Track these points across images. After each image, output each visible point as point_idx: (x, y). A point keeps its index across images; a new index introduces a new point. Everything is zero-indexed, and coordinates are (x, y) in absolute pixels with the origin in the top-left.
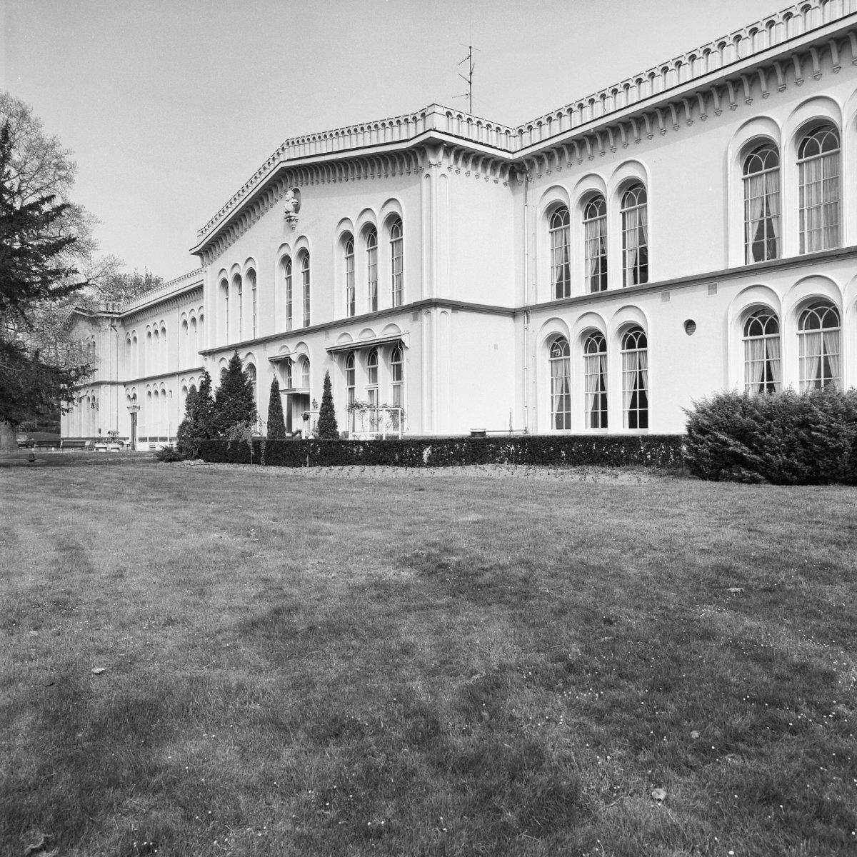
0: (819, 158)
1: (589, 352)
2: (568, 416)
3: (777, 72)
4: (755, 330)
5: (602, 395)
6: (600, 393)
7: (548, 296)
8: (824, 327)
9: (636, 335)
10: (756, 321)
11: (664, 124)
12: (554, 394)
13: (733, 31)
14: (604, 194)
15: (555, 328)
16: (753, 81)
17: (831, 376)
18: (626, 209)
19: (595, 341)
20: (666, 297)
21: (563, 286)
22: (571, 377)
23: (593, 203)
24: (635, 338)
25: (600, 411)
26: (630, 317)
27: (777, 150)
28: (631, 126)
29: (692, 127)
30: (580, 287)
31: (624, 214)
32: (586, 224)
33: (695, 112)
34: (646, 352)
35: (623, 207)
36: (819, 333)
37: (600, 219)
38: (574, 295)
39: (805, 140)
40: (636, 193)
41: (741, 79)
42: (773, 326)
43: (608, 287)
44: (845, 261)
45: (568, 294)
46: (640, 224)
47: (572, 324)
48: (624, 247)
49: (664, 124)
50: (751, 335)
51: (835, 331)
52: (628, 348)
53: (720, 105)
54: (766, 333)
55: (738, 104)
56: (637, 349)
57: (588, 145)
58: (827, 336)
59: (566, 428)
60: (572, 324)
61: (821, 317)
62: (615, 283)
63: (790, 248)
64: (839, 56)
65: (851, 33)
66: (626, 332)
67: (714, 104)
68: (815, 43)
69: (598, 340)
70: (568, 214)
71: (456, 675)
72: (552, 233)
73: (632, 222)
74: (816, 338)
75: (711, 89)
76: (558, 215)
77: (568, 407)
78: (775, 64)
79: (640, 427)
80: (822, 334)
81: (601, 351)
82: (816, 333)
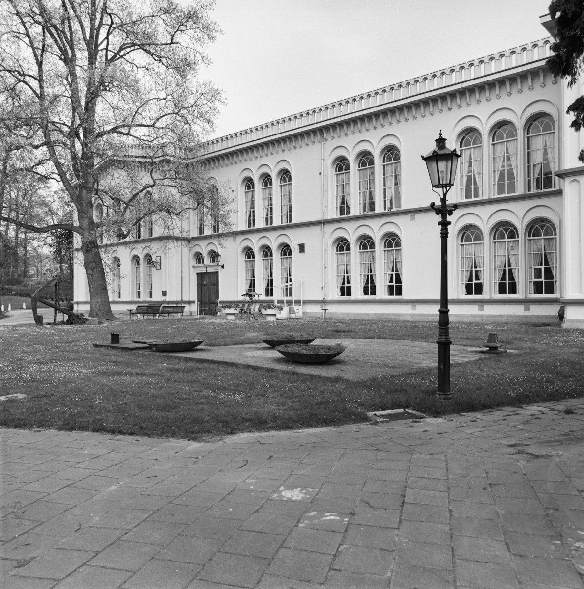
0: (471, 148)
1: (387, 248)
2: (272, 290)
3: (528, 77)
4: (341, 249)
5: (509, 270)
6: (507, 268)
7: (334, 214)
8: (544, 236)
9: (287, 249)
10: (468, 234)
11: (340, 132)
12: (283, 277)
13: (500, 51)
14: (290, 171)
15: (247, 244)
16: (417, 107)
17: (398, 271)
18: (386, 163)
19: (267, 251)
20: (413, 219)
21: (344, 207)
22: (403, 261)
23: (267, 179)
24: (392, 241)
25: (270, 288)
26: (390, 228)
27: (399, 151)
28: (292, 139)
29: (470, 107)
30: (260, 223)
31: (384, 166)
32: (359, 170)
33: (483, 95)
34: (350, 253)
35: (384, 162)
36: (505, 242)
37: (289, 184)
38: (274, 224)
39: (464, 138)
40: (392, 153)
41: (516, 78)
42: (372, 246)
43: (376, 209)
44: (203, 241)
45: (348, 213)
46: (270, 195)
47: (352, 233)
48: (281, 203)
49: (376, 123)
50: (465, 242)
51: (373, 251)
52: (248, 258)
53: (442, 107)
54: (346, 251)
55: (461, 105)
56: (345, 252)
57: (312, 136)
58: (476, 246)
59: (290, 296)
60: (352, 233)
61: (473, 236)
62: (277, 222)
63: (379, 208)
64: (399, 116)
65: (518, 76)
66: (464, 231)
67: (476, 96)
68: (509, 77)
69: (368, 242)
70: (271, 180)
71: (498, 512)
72: (246, 192)
73: (390, 170)
74: (504, 244)
75: (438, 98)
76: (341, 164)
77: (272, 286)
78: (388, 111)
79: (475, 294)
80: (507, 242)
81: (370, 248)
82: (503, 242)
